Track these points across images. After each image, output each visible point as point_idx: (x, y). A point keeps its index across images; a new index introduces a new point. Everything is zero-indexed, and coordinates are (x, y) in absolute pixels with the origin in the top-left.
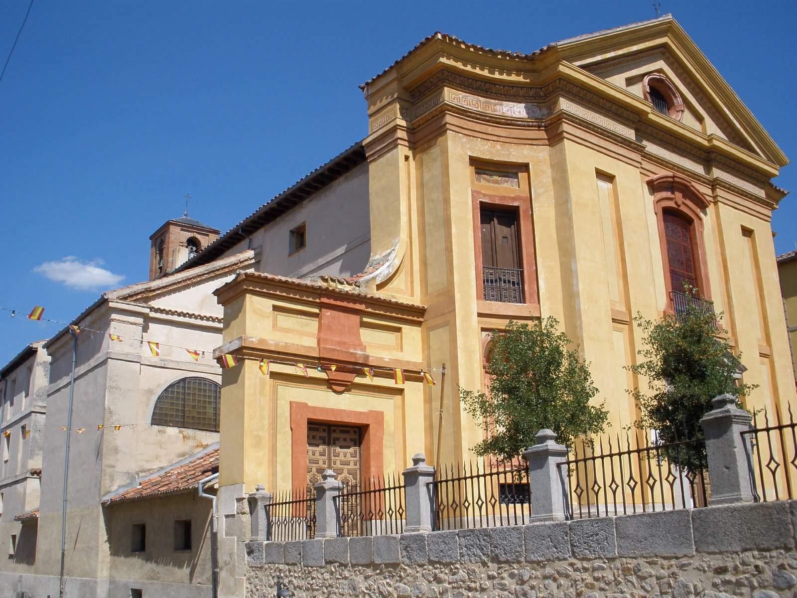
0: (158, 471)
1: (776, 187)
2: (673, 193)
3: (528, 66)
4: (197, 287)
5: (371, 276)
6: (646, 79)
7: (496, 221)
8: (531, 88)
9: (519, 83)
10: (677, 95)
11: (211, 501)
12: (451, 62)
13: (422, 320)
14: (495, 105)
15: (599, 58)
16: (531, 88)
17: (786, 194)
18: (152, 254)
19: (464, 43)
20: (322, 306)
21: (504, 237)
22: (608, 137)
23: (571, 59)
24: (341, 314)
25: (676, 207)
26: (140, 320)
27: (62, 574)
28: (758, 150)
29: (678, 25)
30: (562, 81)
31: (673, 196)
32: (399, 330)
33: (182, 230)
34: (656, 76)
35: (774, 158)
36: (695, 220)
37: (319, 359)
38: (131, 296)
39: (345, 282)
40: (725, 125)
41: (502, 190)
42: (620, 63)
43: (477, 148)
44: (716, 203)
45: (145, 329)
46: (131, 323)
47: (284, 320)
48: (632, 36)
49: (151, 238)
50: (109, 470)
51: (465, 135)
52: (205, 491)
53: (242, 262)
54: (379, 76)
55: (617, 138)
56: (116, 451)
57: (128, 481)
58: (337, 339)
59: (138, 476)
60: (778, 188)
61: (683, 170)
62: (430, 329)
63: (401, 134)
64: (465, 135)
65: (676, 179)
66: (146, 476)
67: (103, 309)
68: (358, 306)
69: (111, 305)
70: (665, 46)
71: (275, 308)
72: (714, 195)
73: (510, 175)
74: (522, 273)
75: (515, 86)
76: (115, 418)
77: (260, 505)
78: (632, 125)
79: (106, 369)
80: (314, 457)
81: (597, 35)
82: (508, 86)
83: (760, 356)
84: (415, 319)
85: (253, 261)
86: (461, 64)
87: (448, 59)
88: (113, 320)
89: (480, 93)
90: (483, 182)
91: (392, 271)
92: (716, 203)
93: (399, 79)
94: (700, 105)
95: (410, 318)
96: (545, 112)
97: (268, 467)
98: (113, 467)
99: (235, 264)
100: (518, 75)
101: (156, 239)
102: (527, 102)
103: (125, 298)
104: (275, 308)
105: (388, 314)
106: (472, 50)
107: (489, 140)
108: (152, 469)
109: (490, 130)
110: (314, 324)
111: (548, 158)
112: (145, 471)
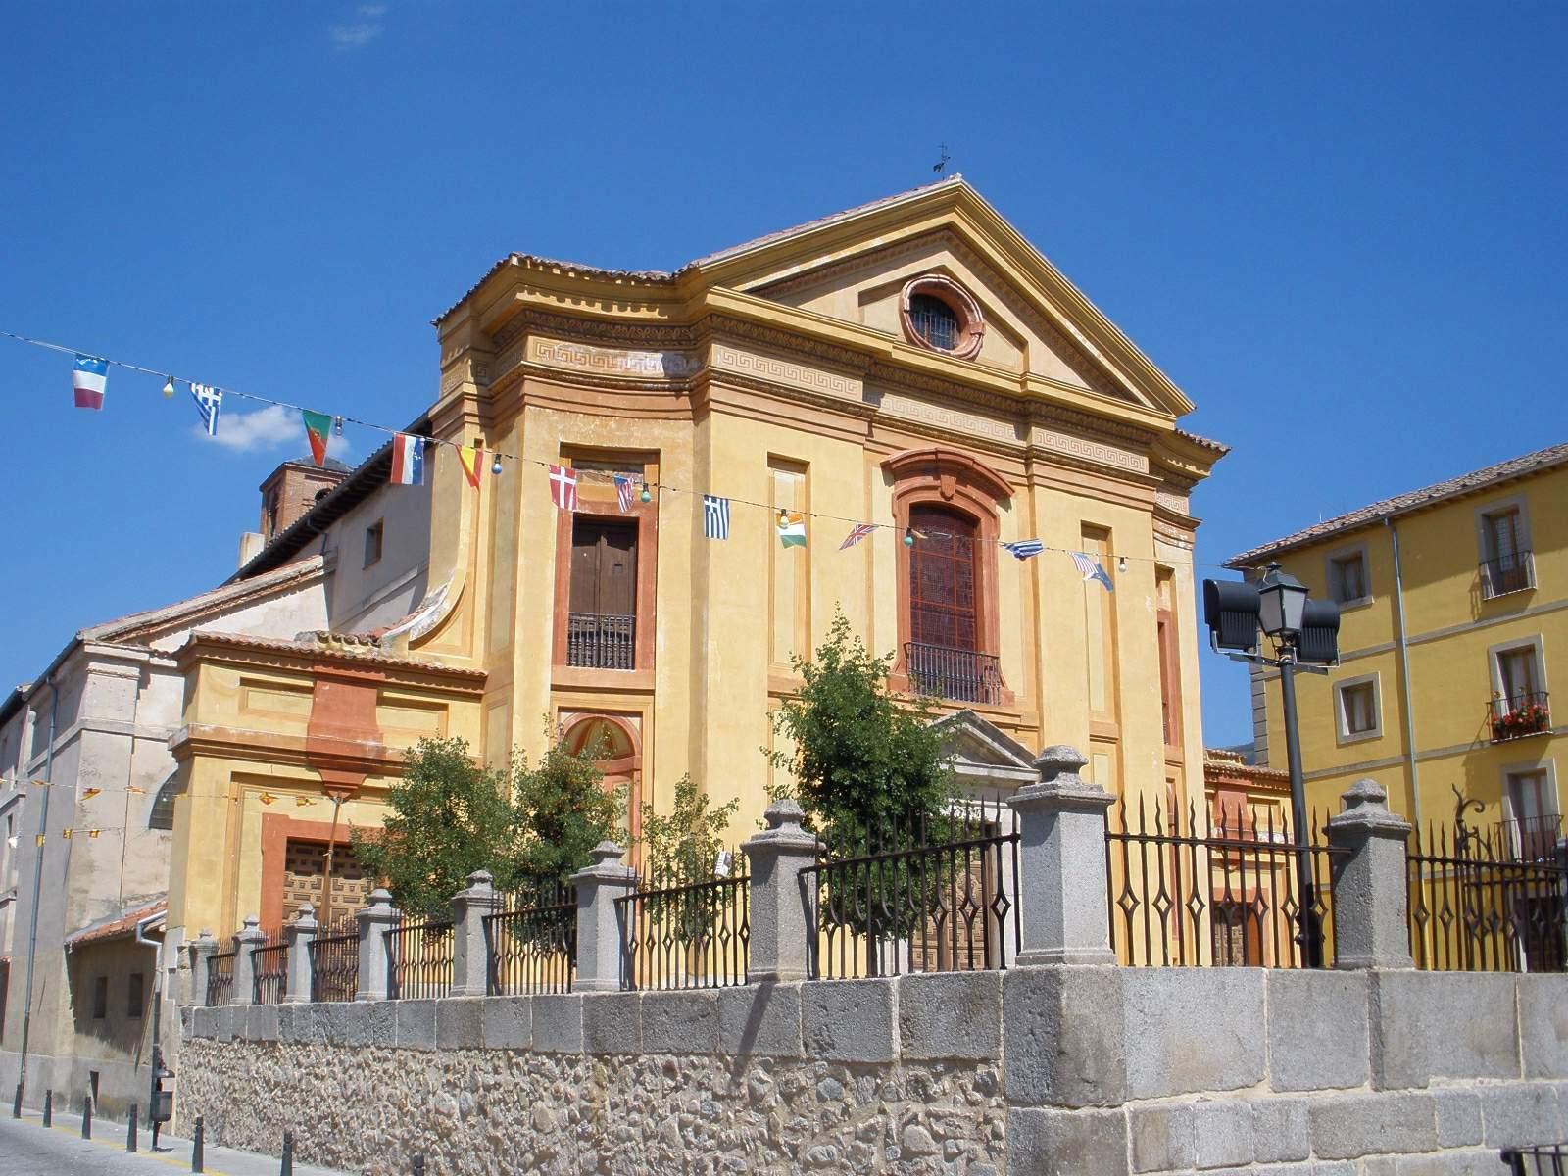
0: (158, 897)
1: (1200, 441)
2: (937, 478)
3: (667, 293)
4: (229, 617)
5: (402, 629)
6: (908, 289)
7: (603, 540)
8: (673, 328)
9: (651, 320)
10: (974, 306)
11: (153, 948)
12: (537, 298)
13: (482, 692)
14: (616, 356)
15: (796, 269)
16: (673, 328)
17: (1225, 453)
18: (263, 515)
20: (317, 677)
21: (617, 565)
22: (803, 400)
23: (728, 282)
24: (348, 688)
25: (943, 500)
26: (135, 671)
27: (25, 1051)
28: (1135, 391)
29: (968, 187)
30: (715, 318)
31: (937, 483)
32: (444, 707)
33: (307, 477)
34: (932, 278)
35: (1166, 403)
36: (982, 520)
37: (307, 753)
38: (119, 635)
39: (356, 641)
41: (603, 494)
42: (842, 271)
43: (576, 429)
44: (1031, 486)
45: (143, 683)
46: (120, 676)
47: (258, 698)
48: (869, 224)
49: (262, 488)
50: (78, 897)
52: (146, 935)
53: (305, 574)
54: (452, 311)
56: (90, 867)
57: (108, 913)
58: (338, 724)
59: (126, 906)
60: (1205, 443)
61: (961, 437)
62: (490, 707)
63: (470, 406)
65: (940, 456)
66: (138, 906)
67: (79, 656)
68: (373, 676)
69: (87, 649)
70: (950, 227)
71: (244, 682)
73: (632, 468)
74: (635, 620)
76: (90, 819)
77: (202, 957)
79: (80, 746)
80: (301, 890)
81: (789, 235)
84: (470, 690)
85: (322, 573)
87: (531, 293)
88: (91, 672)
90: (587, 482)
91: (438, 619)
92: (1031, 486)
93: (476, 318)
95: (461, 689)
96: (694, 363)
97: (223, 904)
98: (86, 891)
99: (293, 579)
101: (269, 491)
103: (110, 638)
104: (244, 682)
105: (424, 685)
106: (572, 275)
108: (148, 895)
109: (600, 399)
110: (305, 703)
111: (691, 440)
112: (136, 899)
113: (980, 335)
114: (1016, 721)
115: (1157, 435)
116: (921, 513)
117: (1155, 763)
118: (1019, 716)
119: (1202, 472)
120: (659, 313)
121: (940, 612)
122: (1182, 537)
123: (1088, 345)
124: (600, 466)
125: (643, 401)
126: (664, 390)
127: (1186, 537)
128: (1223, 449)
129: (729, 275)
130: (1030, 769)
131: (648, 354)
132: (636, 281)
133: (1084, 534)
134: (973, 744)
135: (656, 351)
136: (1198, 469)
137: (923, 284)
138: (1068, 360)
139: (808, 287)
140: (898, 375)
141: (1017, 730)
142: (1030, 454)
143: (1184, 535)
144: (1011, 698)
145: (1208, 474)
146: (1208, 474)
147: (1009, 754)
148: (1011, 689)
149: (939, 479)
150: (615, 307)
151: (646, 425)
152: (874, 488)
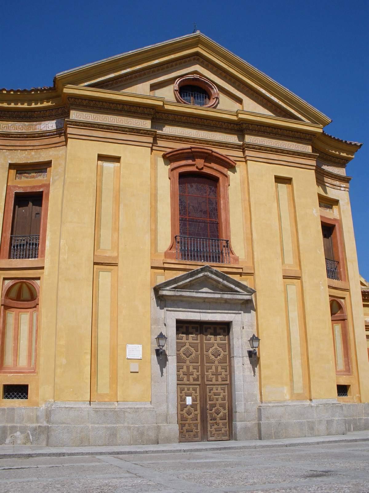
2: (194, 160)
6: (178, 81)
9: (44, 107)
14: (36, 125)
19: (12, 90)
25: (197, 170)
28: (299, 116)
29: (204, 37)
31: (193, 163)
34: (191, 76)
35: (315, 120)
40: (265, 101)
41: (28, 183)
43: (17, 157)
51: (8, 150)
55: (123, 129)
64: (8, 150)
65: (193, 150)
72: (245, 156)
75: (53, 109)
78: (148, 117)
82: (43, 111)
83: (283, 278)
86: (6, 104)
89: (25, 119)
92: (246, 162)
94: (238, 90)
100: (48, 102)
102: (58, 119)
107: (27, 150)
109: (28, 143)
113: (217, 98)
114: (240, 271)
115: (314, 135)
116: (185, 178)
117: (322, 287)
118: (242, 268)
119: (350, 156)
120: (51, 103)
121: (199, 222)
122: (342, 186)
123: (273, 98)
124: (29, 172)
125: (47, 141)
126: (54, 135)
127: (344, 186)
128: (359, 144)
129: (76, 80)
130: (246, 293)
131: (50, 122)
132: (40, 91)
133: (276, 182)
134: (214, 283)
135: (53, 120)
136: (347, 155)
137: (186, 79)
138: (264, 106)
139: (121, 84)
140: (171, 117)
141: (241, 276)
142: (244, 147)
143: (344, 185)
144: (236, 260)
145: (353, 157)
146: (353, 157)
147: (233, 286)
148: (237, 255)
149: (195, 161)
150: (33, 104)
151: (47, 151)
152: (159, 167)
